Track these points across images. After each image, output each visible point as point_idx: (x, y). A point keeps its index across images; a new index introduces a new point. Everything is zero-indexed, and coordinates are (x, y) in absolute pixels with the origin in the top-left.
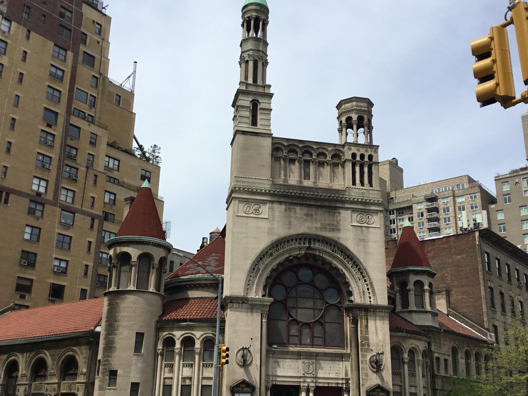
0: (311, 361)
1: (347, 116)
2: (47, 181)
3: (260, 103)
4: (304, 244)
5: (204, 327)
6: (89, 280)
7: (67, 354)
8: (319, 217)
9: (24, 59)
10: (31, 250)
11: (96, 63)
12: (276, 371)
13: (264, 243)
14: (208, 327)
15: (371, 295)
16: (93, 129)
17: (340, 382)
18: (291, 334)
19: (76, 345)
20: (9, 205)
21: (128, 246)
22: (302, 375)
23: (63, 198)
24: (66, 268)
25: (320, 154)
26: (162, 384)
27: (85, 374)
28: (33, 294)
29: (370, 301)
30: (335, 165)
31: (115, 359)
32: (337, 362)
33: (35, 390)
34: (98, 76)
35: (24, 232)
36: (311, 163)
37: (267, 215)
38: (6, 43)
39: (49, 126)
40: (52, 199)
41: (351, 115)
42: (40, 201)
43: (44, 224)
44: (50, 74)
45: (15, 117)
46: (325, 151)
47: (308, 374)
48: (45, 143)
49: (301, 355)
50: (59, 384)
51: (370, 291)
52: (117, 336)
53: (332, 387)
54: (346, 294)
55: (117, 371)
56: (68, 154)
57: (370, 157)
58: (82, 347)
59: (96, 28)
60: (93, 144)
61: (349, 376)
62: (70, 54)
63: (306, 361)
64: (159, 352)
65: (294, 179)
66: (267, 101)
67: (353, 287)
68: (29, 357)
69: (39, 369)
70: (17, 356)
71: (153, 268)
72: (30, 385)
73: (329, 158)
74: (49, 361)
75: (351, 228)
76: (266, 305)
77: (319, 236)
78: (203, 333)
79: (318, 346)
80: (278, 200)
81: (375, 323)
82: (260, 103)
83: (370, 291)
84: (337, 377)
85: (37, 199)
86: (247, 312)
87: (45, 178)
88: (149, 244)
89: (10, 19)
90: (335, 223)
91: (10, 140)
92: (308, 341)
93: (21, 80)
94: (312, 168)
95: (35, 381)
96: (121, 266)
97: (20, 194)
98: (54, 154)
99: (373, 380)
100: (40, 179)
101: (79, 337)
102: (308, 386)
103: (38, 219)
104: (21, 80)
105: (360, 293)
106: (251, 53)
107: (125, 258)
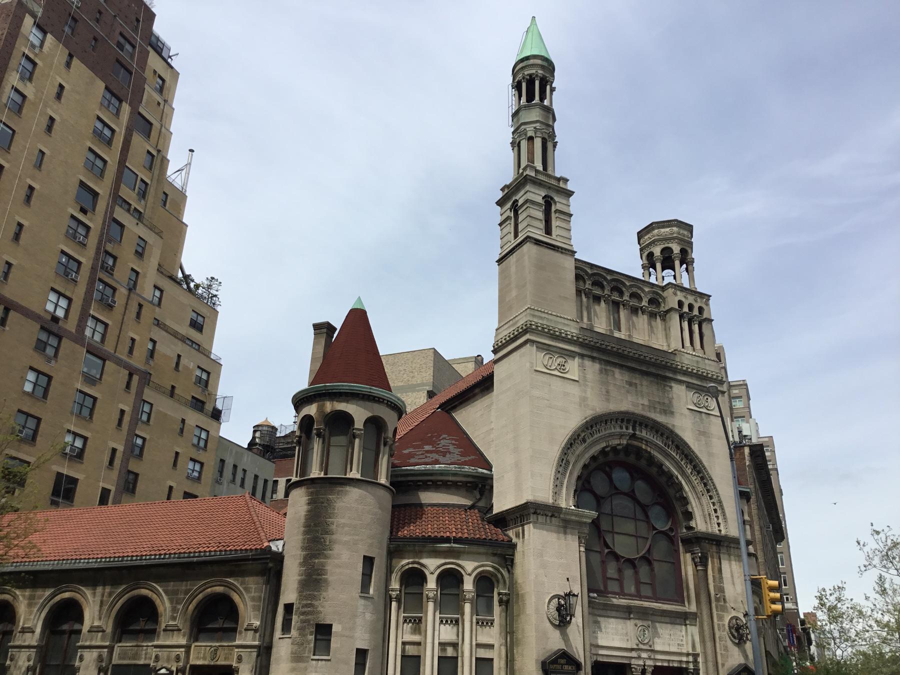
0: (646, 623)
1: (663, 246)
2: (70, 300)
3: (555, 203)
4: (627, 428)
5: (479, 554)
6: (115, 474)
7: (209, 590)
8: (645, 390)
9: (59, 96)
10: (32, 412)
11: (153, 133)
12: (597, 638)
13: (574, 421)
14: (486, 554)
15: (720, 521)
16: (142, 231)
17: (684, 659)
18: (609, 575)
19: (231, 574)
20: (7, 328)
21: (347, 402)
22: (635, 647)
23: (88, 332)
24: (82, 451)
25: (633, 295)
26: (399, 653)
27: (256, 631)
28: (28, 489)
29: (720, 531)
30: (653, 315)
31: (326, 604)
32: (678, 627)
33: (120, 658)
34: (154, 153)
35: (24, 379)
36: (621, 306)
37: (577, 374)
38: (34, 64)
39: (83, 211)
40: (74, 331)
41: (670, 245)
42: (56, 331)
43: (58, 370)
44: (94, 131)
45: (34, 185)
46: (639, 292)
47: (644, 644)
48: (72, 236)
49: (630, 613)
50: (188, 648)
51: (719, 513)
52: (329, 561)
53: (673, 667)
54: (681, 516)
55: (331, 626)
56: (105, 261)
57: (701, 310)
58: (247, 579)
59: (158, 83)
60: (140, 255)
61: (699, 650)
62: (126, 108)
63: (640, 623)
64: (394, 594)
65: (601, 325)
66: (564, 202)
67: (694, 506)
68: (110, 594)
69: (136, 619)
70: (78, 591)
71: (385, 445)
72: (111, 649)
73: (644, 303)
74: (164, 605)
75: (687, 412)
76: (585, 523)
77: (648, 418)
78: (476, 564)
79: (647, 598)
80: (589, 353)
81: (730, 566)
82: (555, 203)
83: (719, 513)
84: (679, 651)
85: (51, 326)
86: (558, 532)
87: (68, 294)
88: (383, 402)
89: (45, 28)
90: (666, 401)
91: (22, 221)
92: (633, 590)
93: (49, 128)
94: (623, 314)
95: (120, 642)
96: (331, 435)
97: (27, 313)
98: (86, 259)
99: (735, 658)
100: (60, 294)
101: (246, 559)
102: (644, 666)
103: (49, 360)
104: (49, 128)
105: (705, 517)
106: (538, 125)
107: (342, 421)
